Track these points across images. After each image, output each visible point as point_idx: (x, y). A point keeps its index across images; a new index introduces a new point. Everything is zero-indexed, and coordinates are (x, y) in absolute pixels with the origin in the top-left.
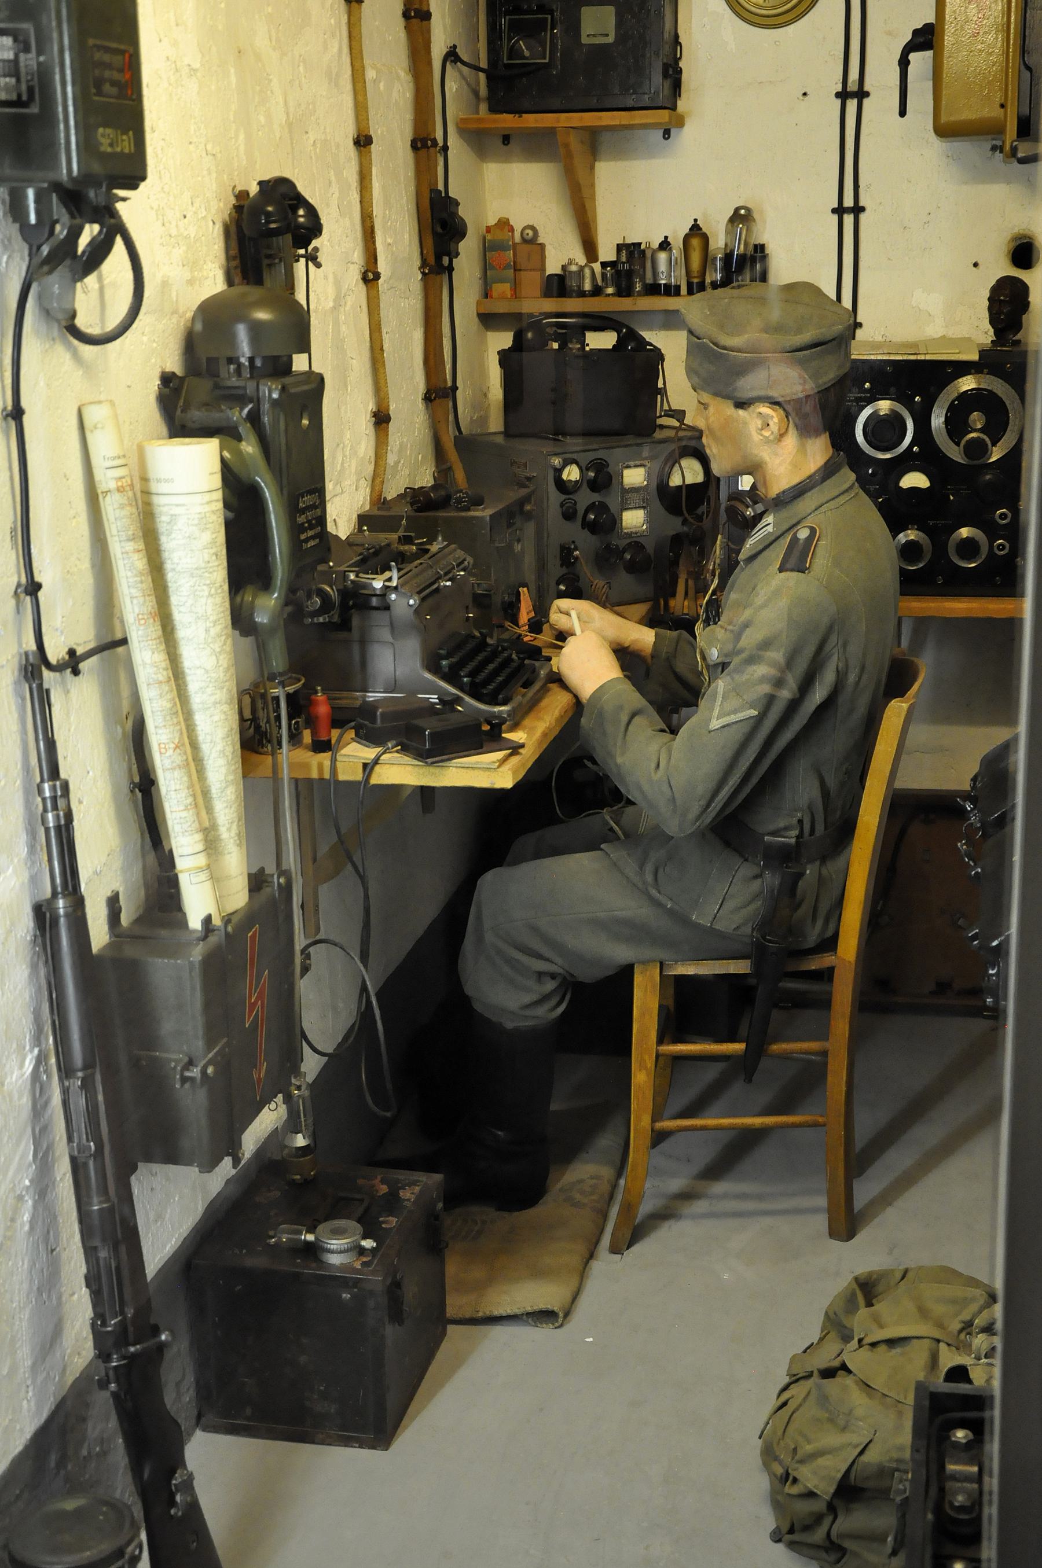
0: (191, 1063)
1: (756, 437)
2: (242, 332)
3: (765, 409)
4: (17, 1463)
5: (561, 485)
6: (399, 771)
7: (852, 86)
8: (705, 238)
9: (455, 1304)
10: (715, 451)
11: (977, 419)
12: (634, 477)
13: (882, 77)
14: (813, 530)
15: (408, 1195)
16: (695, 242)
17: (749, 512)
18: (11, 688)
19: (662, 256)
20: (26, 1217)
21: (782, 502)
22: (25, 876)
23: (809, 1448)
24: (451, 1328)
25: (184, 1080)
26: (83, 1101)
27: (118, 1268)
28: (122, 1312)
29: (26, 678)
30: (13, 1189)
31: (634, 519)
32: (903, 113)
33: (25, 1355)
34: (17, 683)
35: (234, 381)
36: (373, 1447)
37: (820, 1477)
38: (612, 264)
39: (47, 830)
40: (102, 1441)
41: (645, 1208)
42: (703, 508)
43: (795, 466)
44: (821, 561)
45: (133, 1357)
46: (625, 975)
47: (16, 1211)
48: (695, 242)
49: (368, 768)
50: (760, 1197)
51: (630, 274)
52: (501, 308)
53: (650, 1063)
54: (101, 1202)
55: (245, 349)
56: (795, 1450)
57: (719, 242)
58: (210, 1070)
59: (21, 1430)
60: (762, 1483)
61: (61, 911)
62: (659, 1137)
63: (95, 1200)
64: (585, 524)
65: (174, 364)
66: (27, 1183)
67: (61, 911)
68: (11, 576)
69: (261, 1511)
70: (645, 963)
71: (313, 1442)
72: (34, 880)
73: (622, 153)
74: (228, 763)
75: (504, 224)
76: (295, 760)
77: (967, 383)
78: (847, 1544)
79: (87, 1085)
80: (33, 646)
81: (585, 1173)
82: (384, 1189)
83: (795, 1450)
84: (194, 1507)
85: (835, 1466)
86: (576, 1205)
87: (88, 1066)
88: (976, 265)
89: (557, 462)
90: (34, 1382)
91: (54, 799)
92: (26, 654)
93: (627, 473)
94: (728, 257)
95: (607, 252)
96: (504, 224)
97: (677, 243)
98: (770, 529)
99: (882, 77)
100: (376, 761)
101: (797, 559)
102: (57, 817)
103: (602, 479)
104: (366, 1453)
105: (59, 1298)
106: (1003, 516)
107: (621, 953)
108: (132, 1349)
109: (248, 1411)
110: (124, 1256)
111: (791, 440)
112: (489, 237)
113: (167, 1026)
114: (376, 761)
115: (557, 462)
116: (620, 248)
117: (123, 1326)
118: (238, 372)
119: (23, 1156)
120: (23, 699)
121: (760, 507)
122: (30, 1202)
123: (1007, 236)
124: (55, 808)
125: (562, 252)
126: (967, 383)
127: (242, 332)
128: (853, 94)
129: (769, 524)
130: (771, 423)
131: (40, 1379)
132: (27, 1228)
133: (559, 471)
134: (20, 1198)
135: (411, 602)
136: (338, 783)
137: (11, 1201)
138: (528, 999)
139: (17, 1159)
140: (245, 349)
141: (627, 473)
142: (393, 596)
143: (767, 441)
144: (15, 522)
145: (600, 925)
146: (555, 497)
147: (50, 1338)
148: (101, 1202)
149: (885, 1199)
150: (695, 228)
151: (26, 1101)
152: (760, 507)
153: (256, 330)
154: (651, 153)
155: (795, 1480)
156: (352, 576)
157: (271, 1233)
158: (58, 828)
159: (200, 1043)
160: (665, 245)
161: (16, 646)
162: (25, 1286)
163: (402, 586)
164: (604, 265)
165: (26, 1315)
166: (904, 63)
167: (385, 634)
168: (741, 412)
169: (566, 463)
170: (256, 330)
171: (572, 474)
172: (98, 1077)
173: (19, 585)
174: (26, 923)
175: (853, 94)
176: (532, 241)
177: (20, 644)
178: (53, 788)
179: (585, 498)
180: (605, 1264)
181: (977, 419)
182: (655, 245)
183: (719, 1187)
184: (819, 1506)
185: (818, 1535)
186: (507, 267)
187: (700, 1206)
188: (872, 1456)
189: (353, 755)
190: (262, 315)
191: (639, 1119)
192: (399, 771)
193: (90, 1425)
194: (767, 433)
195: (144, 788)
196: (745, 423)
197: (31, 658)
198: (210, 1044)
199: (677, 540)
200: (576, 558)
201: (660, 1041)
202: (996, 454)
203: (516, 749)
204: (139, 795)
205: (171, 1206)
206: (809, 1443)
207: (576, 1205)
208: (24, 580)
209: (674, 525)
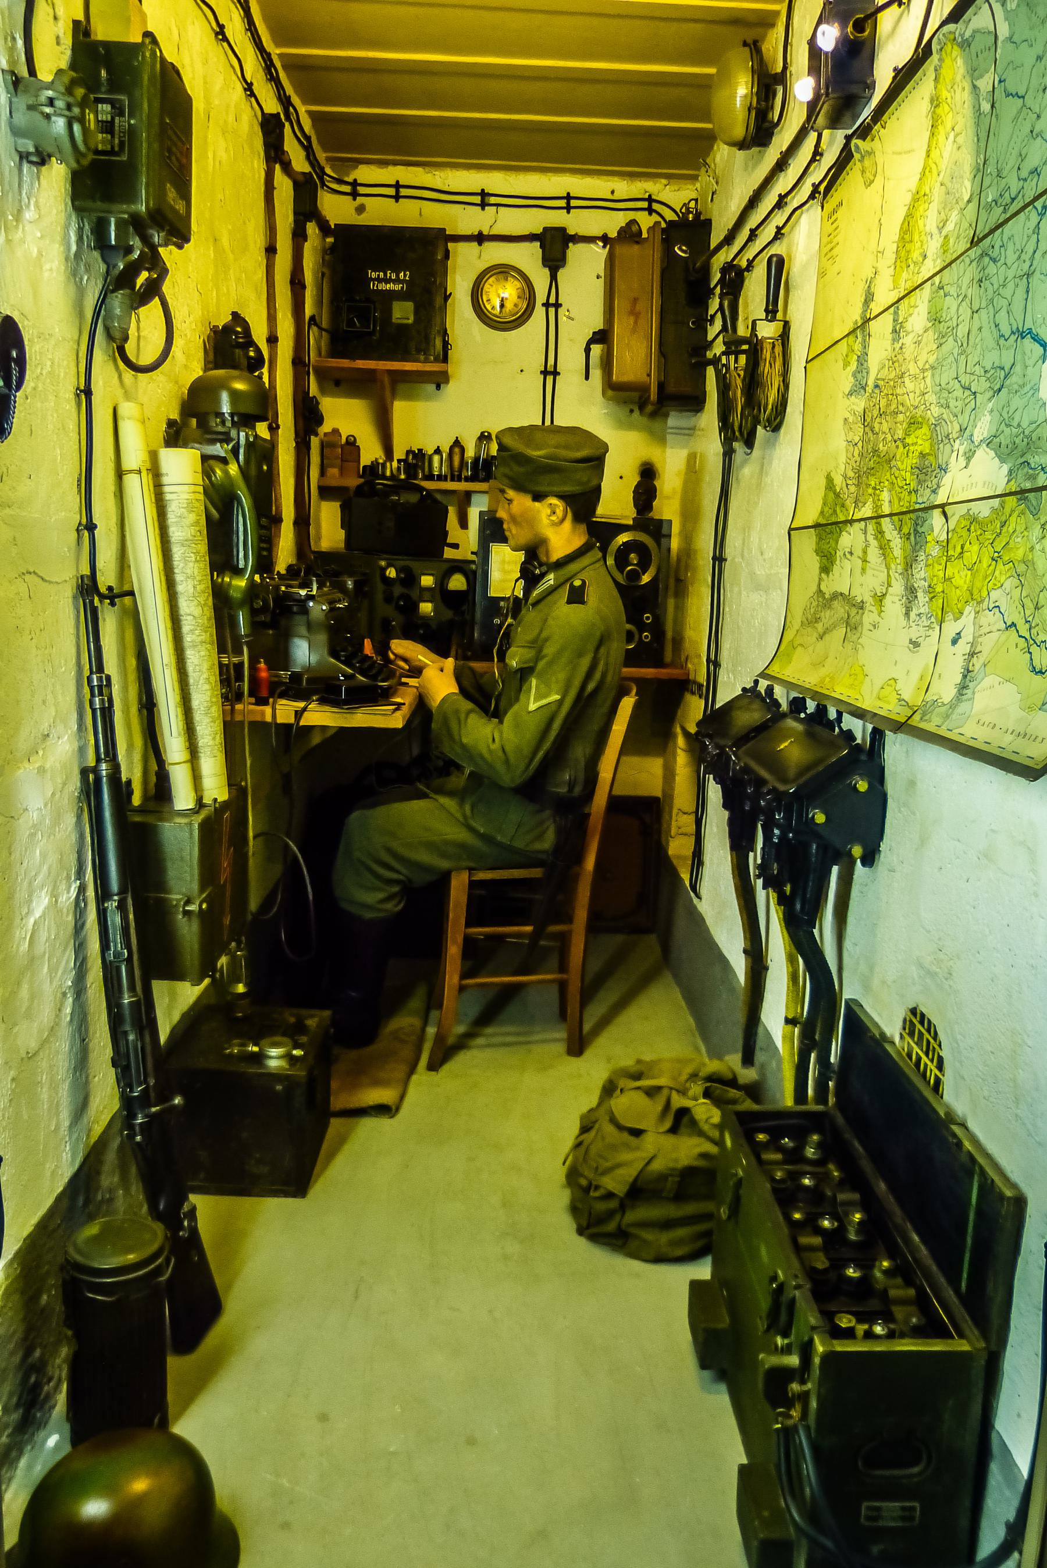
0: (188, 902)
1: (545, 521)
2: (225, 397)
3: (554, 501)
4: (59, 1199)
5: (386, 580)
6: (320, 716)
7: (550, 368)
8: (463, 450)
9: (338, 1102)
10: (514, 531)
11: (633, 557)
12: (427, 581)
13: (571, 358)
14: (584, 582)
15: (312, 1023)
16: (457, 450)
17: (537, 571)
18: (70, 600)
19: (436, 458)
20: (68, 1010)
21: (559, 565)
22: (76, 745)
23: (608, 1164)
24: (333, 1121)
25: (187, 913)
26: (118, 919)
27: (143, 1048)
28: (146, 1081)
29: (81, 593)
30: (61, 986)
31: (426, 608)
32: (587, 378)
33: (65, 1117)
34: (75, 597)
35: (220, 429)
36: (295, 1196)
37: (616, 1183)
38: (405, 461)
39: (94, 711)
40: (110, 1191)
41: (451, 1040)
42: (465, 608)
43: (569, 541)
44: (592, 596)
45: (152, 1117)
46: (444, 879)
47: (62, 1004)
48: (457, 450)
49: (299, 714)
50: (518, 1034)
51: (415, 466)
52: (334, 483)
53: (460, 939)
54: (130, 997)
55: (226, 409)
56: (597, 1168)
57: (470, 453)
58: (204, 906)
59: (62, 1175)
60: (565, 1197)
61: (104, 773)
62: (462, 989)
63: (126, 996)
64: (398, 608)
65: (175, 415)
66: (70, 984)
67: (104, 773)
68: (74, 515)
69: (232, 1236)
70: (459, 869)
71: (249, 1195)
72: (82, 750)
73: (410, 397)
74: (212, 689)
75: (336, 432)
76: (247, 709)
77: (623, 538)
78: (633, 1230)
79: (122, 907)
80: (86, 571)
81: (404, 1022)
82: (292, 1020)
83: (597, 1168)
84: (194, 1231)
85: (629, 1173)
86: (402, 1041)
87: (122, 891)
88: (621, 477)
89: (383, 563)
90: (70, 1138)
91: (100, 687)
92: (82, 577)
93: (423, 578)
94: (476, 459)
95: (399, 453)
96: (336, 432)
97: (445, 450)
98: (552, 582)
99: (571, 358)
100: (304, 709)
101: (577, 596)
102: (102, 701)
103: (409, 579)
104: (290, 1200)
105: (87, 1077)
106: (648, 618)
107: (445, 864)
108: (153, 1109)
109: (202, 1175)
110: (147, 1039)
111: (568, 524)
112: (326, 439)
113: (173, 873)
114: (304, 709)
115: (383, 563)
116: (408, 452)
117: (145, 1092)
118: (223, 422)
119: (67, 962)
120: (78, 612)
121: (544, 569)
122: (71, 1000)
123: (638, 463)
124: (101, 694)
125: (370, 452)
126: (623, 538)
127: (225, 397)
128: (551, 372)
129: (551, 579)
130: (558, 511)
131: (75, 1136)
132: (68, 1019)
133: (384, 570)
134: (64, 994)
135: (324, 608)
136: (277, 724)
137: (59, 995)
138: (381, 895)
139: (64, 963)
140: (226, 409)
141: (423, 578)
142: (311, 604)
143: (554, 524)
144: (80, 474)
145: (431, 846)
146: (380, 587)
147: (81, 1106)
148: (130, 997)
149: (604, 1022)
150: (457, 443)
151: (70, 918)
152: (544, 569)
153: (235, 395)
154: (428, 398)
155: (597, 1188)
156: (283, 588)
157: (226, 1046)
158: (103, 709)
159: (195, 886)
160: (438, 451)
161: (75, 569)
162: (67, 1064)
163: (319, 596)
164: (399, 461)
165: (66, 1086)
166: (588, 350)
167: (303, 630)
168: (537, 504)
169: (389, 565)
170: (235, 395)
171: (392, 573)
172: (130, 901)
173: (80, 524)
174: (75, 783)
175: (551, 372)
176: (352, 444)
177: (78, 570)
178: (100, 679)
179: (398, 590)
180: (421, 1077)
181: (633, 557)
182: (430, 452)
183: (489, 1030)
184: (613, 1204)
185: (611, 1227)
186: (337, 458)
187: (480, 1041)
188: (657, 1166)
189: (284, 711)
190: (239, 386)
191: (451, 978)
192: (320, 716)
193: (103, 1177)
194: (554, 518)
195: (148, 705)
196: (539, 511)
197: (86, 581)
198: (202, 890)
199: (451, 623)
200: (393, 626)
201: (468, 925)
202: (646, 579)
203: (399, 706)
204: (145, 712)
205: (176, 1000)
206: (606, 1160)
207: (402, 1041)
208: (84, 521)
209: (448, 614)
